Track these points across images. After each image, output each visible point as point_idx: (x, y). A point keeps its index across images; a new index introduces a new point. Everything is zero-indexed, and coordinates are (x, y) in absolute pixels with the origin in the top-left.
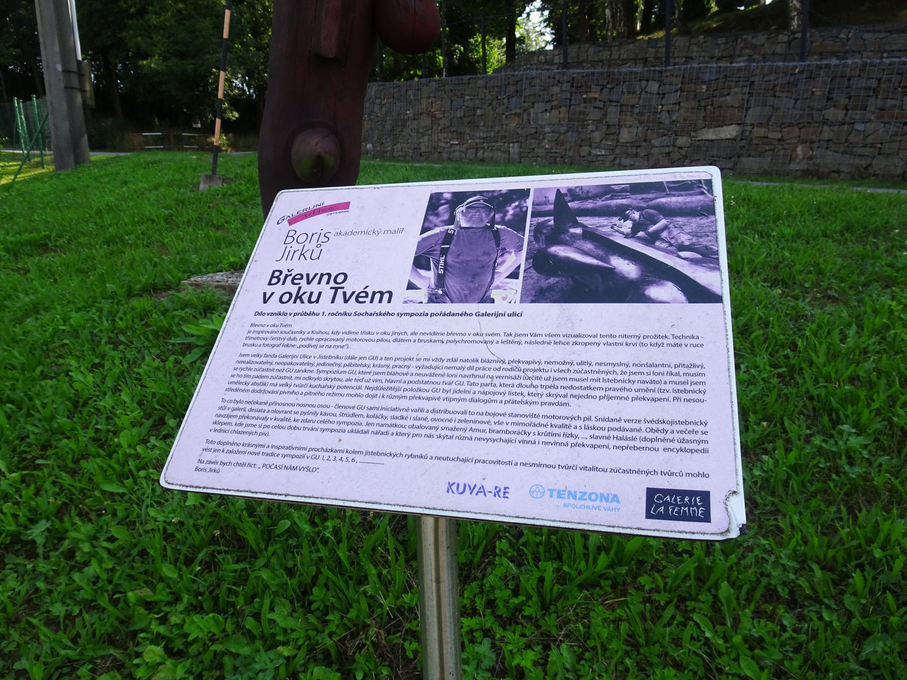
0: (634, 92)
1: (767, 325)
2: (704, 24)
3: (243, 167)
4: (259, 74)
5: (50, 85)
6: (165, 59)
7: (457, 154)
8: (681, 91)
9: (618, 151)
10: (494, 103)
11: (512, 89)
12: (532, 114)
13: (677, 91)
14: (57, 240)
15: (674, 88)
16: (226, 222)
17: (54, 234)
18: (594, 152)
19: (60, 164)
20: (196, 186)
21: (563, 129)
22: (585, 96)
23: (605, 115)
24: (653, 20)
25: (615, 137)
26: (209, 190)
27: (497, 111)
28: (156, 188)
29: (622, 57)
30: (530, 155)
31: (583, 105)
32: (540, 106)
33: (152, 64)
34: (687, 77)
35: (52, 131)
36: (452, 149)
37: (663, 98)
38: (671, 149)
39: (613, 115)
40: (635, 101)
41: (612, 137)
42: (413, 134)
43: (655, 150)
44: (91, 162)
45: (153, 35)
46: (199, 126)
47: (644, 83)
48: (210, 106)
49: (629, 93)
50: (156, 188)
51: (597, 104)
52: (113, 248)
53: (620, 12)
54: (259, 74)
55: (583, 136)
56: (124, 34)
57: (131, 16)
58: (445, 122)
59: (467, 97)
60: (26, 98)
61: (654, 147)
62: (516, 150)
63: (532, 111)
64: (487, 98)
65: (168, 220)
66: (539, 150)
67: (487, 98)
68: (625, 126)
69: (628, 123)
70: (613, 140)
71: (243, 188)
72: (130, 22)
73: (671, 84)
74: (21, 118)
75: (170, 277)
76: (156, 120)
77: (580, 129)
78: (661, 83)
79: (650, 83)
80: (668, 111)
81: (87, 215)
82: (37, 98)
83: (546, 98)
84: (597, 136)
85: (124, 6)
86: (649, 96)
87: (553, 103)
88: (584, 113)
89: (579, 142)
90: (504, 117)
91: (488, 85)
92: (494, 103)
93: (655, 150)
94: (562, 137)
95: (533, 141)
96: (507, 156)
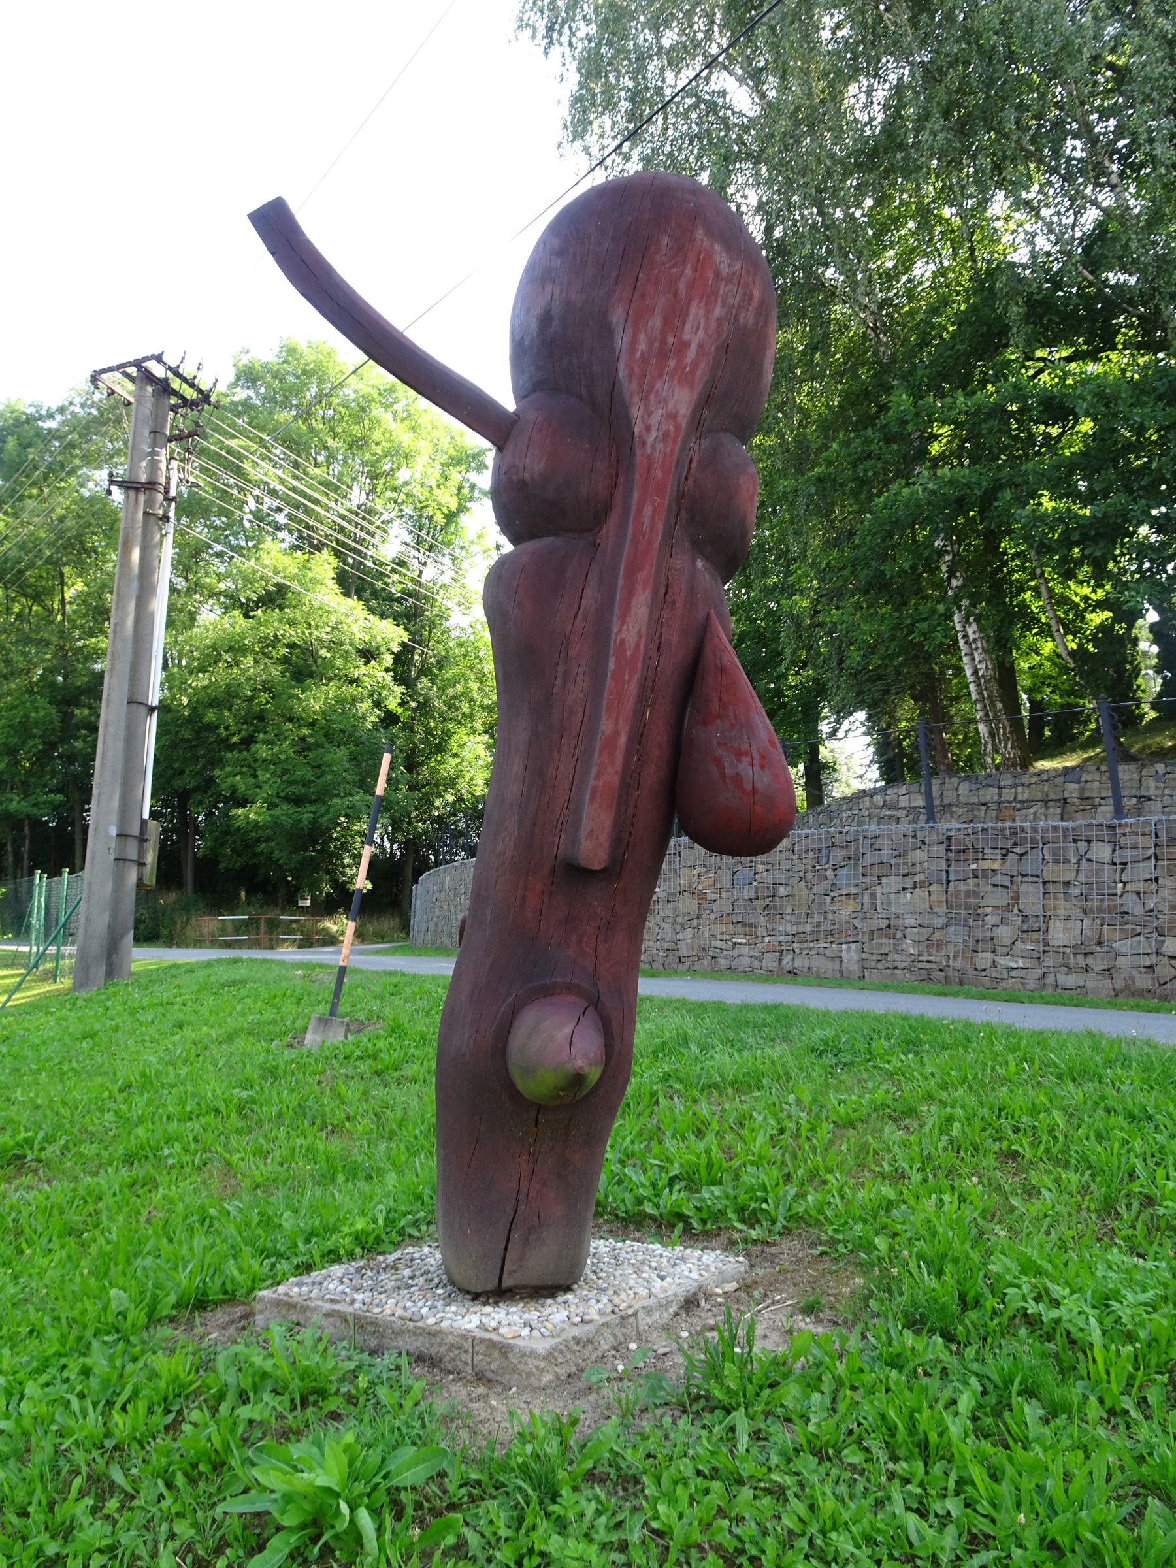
0: (1067, 861)
1: (465, 656)
2: (1149, 741)
3: (380, 997)
4: (409, 823)
5: (93, 859)
6: (271, 806)
7: (746, 961)
8: (1157, 859)
9: (1048, 961)
10: (809, 876)
11: (838, 854)
12: (879, 896)
13: (1149, 858)
14: (42, 1149)
15: (1141, 854)
16: (348, 1118)
17: (41, 1134)
18: (1001, 961)
19: (82, 979)
20: (297, 1039)
21: (939, 921)
22: (974, 866)
23: (1017, 897)
24: (1048, 733)
25: (1040, 935)
26: (321, 1048)
27: (815, 890)
28: (231, 1038)
29: (1020, 797)
30: (880, 965)
31: (972, 881)
32: (892, 883)
33: (252, 814)
34: (1163, 834)
35: (82, 924)
36: (735, 953)
37: (1123, 870)
38: (1154, 959)
39: (1031, 898)
40: (1069, 876)
41: (1034, 936)
42: (665, 925)
43: (1121, 961)
44: (131, 974)
45: (259, 773)
46: (308, 903)
47: (1082, 846)
48: (328, 873)
49: (1056, 861)
50: (231, 1038)
51: (998, 879)
52: (138, 1171)
53: (1004, 728)
54: (409, 823)
55: (979, 934)
56: (217, 772)
57: (231, 748)
58: (722, 906)
59: (761, 867)
60: (54, 873)
61: (1117, 955)
62: (855, 956)
63: (878, 889)
64: (796, 868)
65: (243, 1110)
66: (897, 957)
67: (796, 868)
68: (1057, 918)
69: (1061, 912)
70: (1037, 941)
71: (381, 1044)
72: (229, 755)
73: (1134, 847)
74: (39, 901)
75: (236, 1273)
76: (243, 894)
77: (971, 922)
78: (1115, 846)
79: (1094, 844)
80: (1138, 894)
81: (106, 1094)
82: (70, 873)
83: (903, 870)
84: (1005, 934)
85: (224, 734)
86: (1095, 867)
87: (916, 878)
88: (975, 894)
89: (972, 944)
90: (828, 899)
91: (796, 848)
92: (809, 876)
93: (1121, 961)
94: (937, 936)
95: (884, 940)
96: (837, 967)
